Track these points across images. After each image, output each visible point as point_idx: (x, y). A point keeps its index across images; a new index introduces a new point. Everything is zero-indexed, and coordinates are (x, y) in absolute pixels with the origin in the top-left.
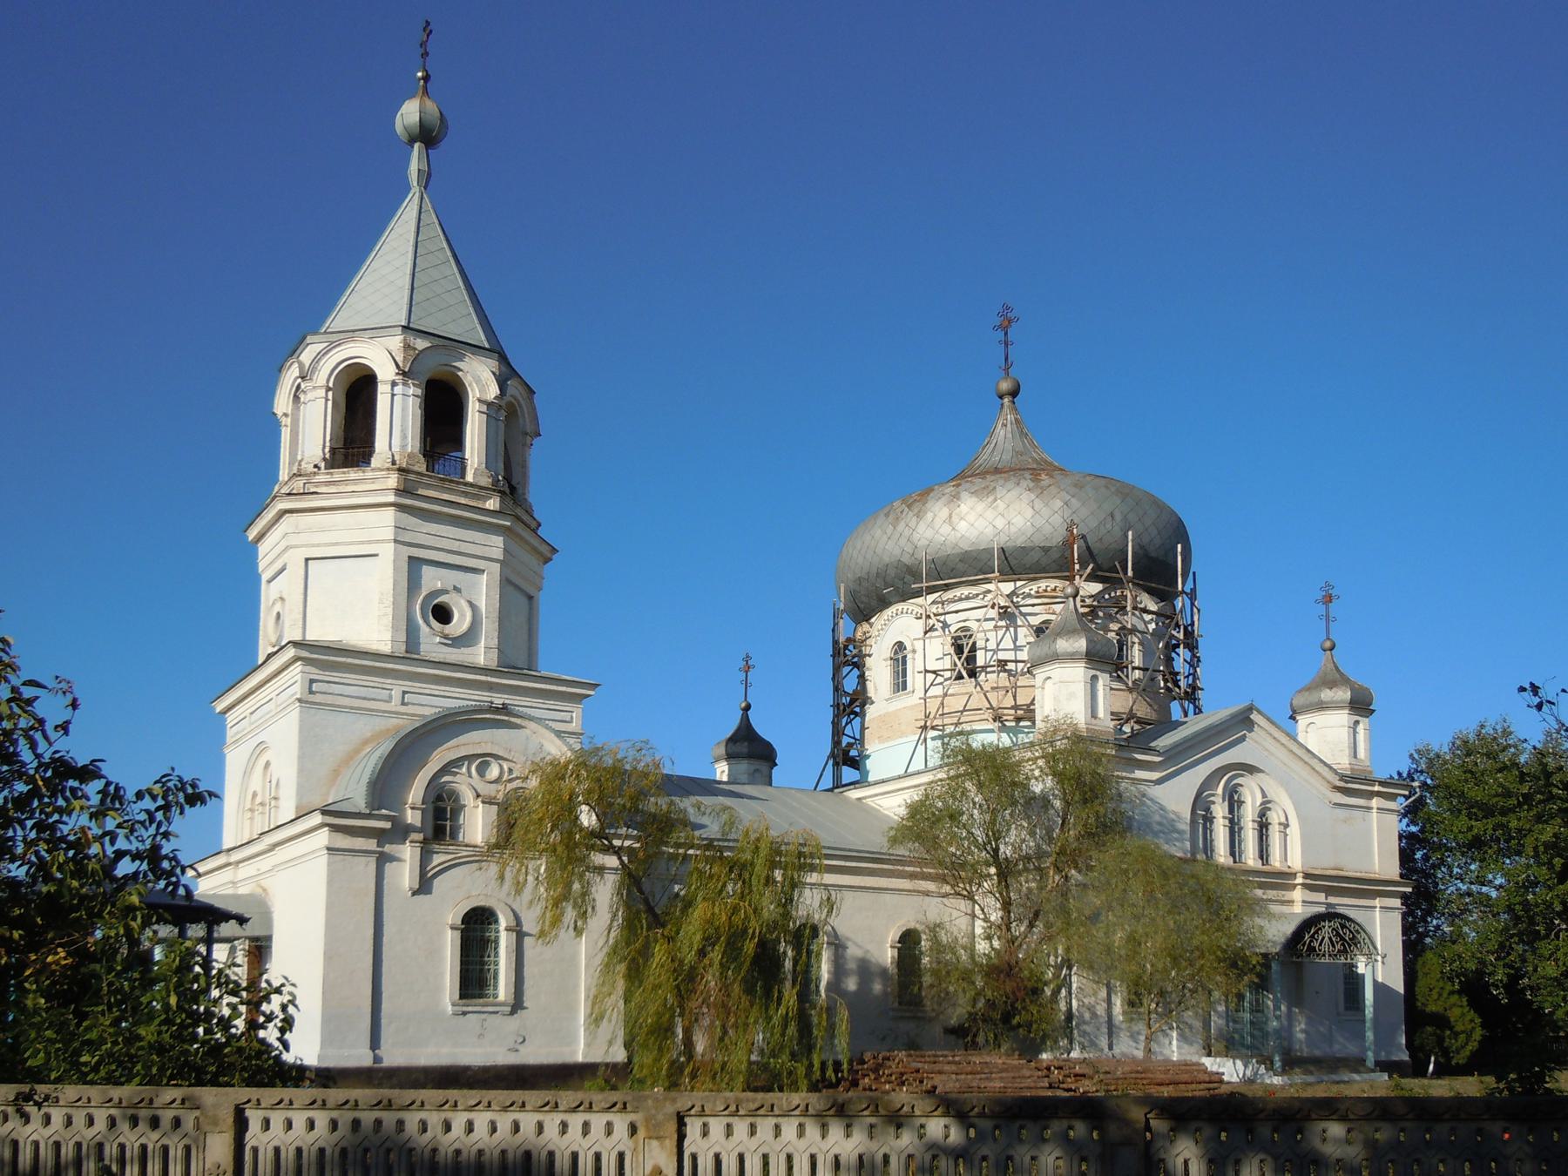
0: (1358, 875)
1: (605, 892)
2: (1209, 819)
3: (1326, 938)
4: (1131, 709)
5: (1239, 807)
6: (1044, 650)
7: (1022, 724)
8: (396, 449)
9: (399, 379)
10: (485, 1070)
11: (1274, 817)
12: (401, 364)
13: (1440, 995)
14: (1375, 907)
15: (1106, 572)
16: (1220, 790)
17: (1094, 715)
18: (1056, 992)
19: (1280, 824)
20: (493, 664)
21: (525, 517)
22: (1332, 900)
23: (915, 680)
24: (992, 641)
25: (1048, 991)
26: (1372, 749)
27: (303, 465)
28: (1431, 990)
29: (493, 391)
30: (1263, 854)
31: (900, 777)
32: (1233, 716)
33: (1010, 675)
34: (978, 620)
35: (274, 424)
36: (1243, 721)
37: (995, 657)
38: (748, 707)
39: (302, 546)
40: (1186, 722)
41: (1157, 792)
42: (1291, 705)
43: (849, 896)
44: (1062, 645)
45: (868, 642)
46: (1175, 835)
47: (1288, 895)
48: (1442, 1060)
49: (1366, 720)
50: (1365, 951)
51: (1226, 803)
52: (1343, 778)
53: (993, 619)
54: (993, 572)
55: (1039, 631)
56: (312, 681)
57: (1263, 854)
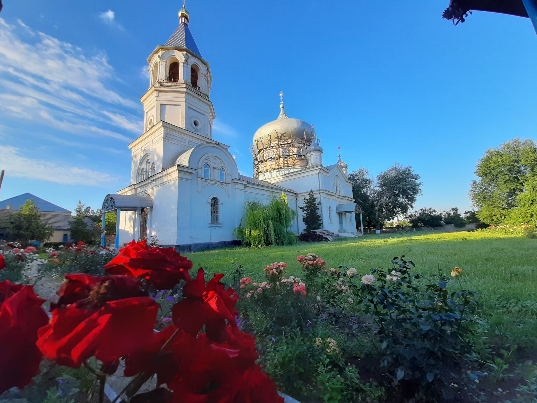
10: (220, 243)
39: (159, 100)
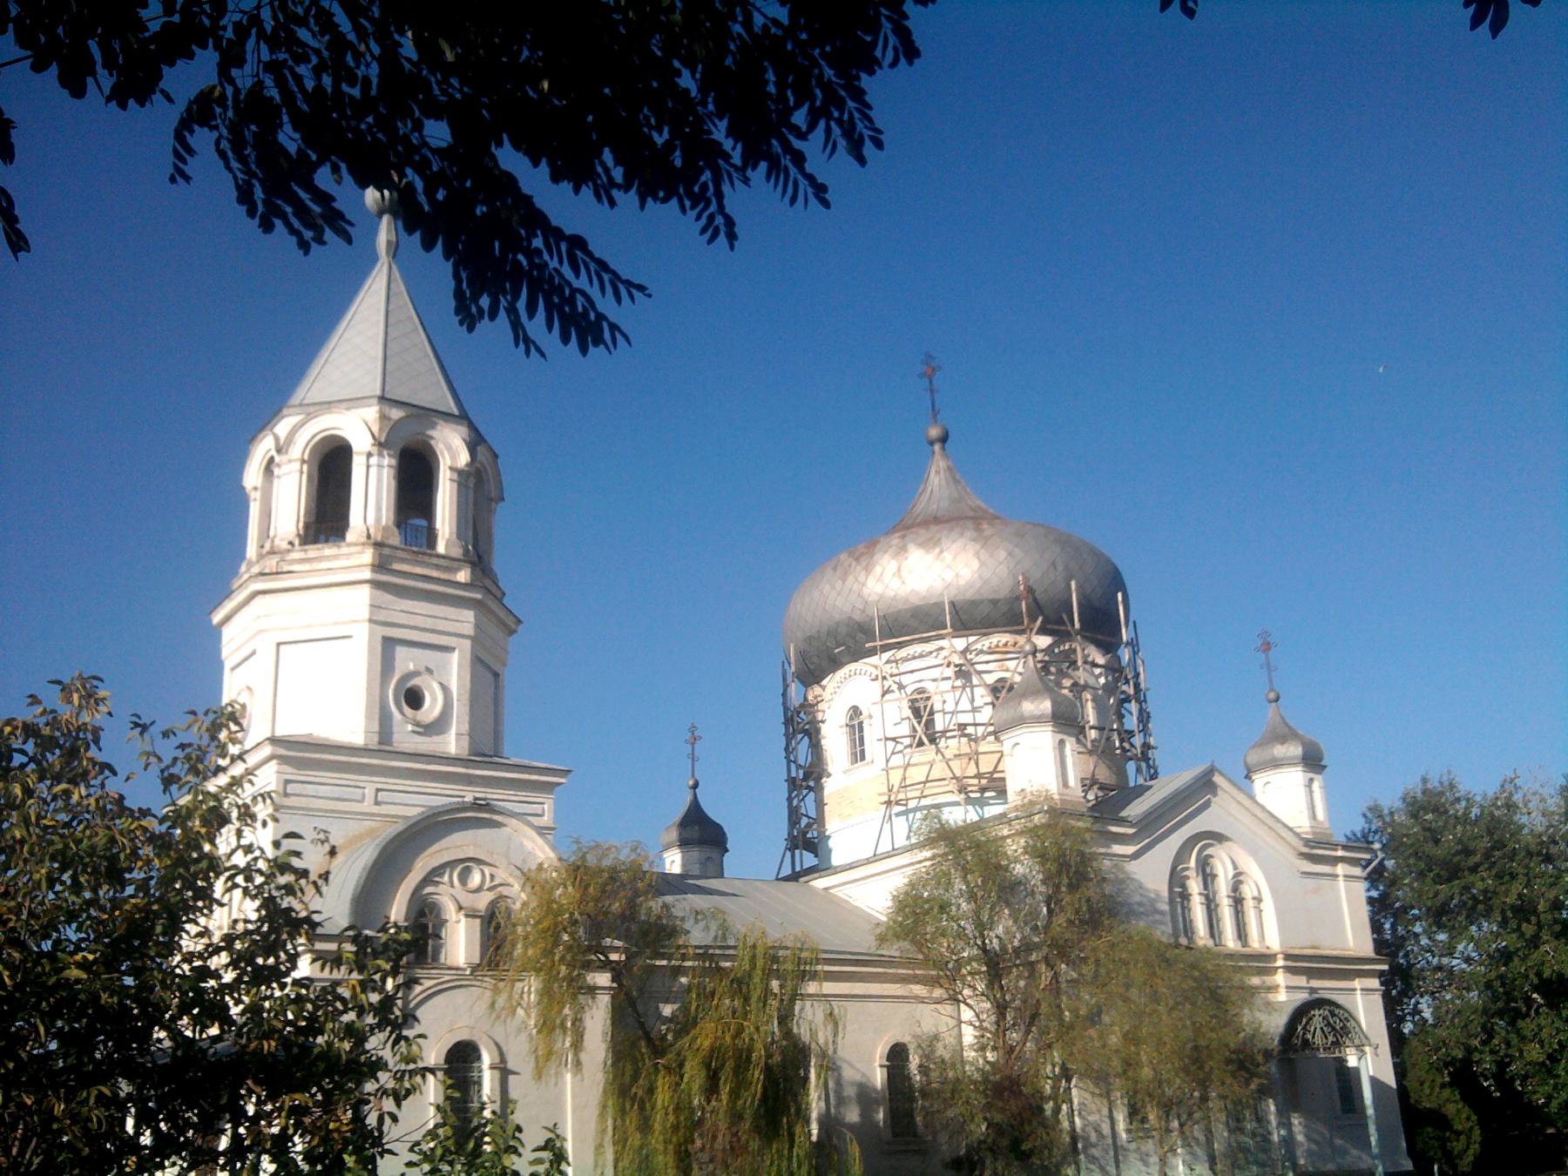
0: (1335, 953)
1: (598, 1019)
2: (1185, 896)
3: (1318, 1030)
4: (1093, 775)
5: (1213, 882)
6: (1006, 714)
7: (987, 794)
8: (371, 520)
9: (375, 450)
11: (1248, 891)
12: (376, 434)
13: (1432, 1089)
14: (1355, 990)
15: (1055, 624)
16: (1193, 863)
17: (1065, 784)
18: (1057, 1110)
19: (1254, 898)
20: (464, 753)
21: (493, 588)
22: (1315, 983)
23: (873, 747)
24: (949, 703)
25: (1049, 1107)
26: (1330, 808)
27: (277, 542)
28: (1422, 1084)
29: (464, 458)
30: (1242, 933)
31: (868, 862)
32: (1197, 779)
33: (970, 740)
34: (934, 680)
35: (240, 500)
36: (1204, 785)
37: (954, 721)
38: (695, 786)
40: (1151, 787)
41: (1133, 868)
42: (1245, 762)
43: (853, 1008)
44: (1028, 707)
45: (820, 706)
46: (1157, 917)
47: (1268, 980)
48: (1445, 1168)
49: (1320, 777)
50: (1357, 1042)
51: (1200, 878)
52: (1307, 842)
53: (949, 678)
54: (945, 628)
55: (995, 690)
56: (287, 782)
57: (1242, 933)
